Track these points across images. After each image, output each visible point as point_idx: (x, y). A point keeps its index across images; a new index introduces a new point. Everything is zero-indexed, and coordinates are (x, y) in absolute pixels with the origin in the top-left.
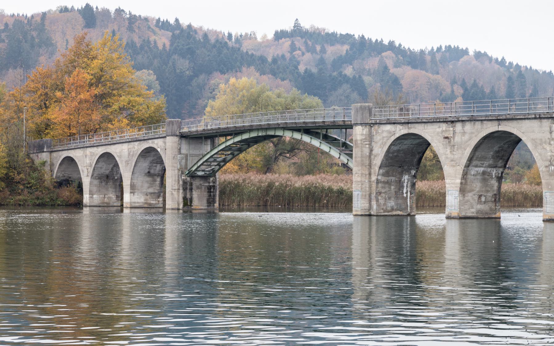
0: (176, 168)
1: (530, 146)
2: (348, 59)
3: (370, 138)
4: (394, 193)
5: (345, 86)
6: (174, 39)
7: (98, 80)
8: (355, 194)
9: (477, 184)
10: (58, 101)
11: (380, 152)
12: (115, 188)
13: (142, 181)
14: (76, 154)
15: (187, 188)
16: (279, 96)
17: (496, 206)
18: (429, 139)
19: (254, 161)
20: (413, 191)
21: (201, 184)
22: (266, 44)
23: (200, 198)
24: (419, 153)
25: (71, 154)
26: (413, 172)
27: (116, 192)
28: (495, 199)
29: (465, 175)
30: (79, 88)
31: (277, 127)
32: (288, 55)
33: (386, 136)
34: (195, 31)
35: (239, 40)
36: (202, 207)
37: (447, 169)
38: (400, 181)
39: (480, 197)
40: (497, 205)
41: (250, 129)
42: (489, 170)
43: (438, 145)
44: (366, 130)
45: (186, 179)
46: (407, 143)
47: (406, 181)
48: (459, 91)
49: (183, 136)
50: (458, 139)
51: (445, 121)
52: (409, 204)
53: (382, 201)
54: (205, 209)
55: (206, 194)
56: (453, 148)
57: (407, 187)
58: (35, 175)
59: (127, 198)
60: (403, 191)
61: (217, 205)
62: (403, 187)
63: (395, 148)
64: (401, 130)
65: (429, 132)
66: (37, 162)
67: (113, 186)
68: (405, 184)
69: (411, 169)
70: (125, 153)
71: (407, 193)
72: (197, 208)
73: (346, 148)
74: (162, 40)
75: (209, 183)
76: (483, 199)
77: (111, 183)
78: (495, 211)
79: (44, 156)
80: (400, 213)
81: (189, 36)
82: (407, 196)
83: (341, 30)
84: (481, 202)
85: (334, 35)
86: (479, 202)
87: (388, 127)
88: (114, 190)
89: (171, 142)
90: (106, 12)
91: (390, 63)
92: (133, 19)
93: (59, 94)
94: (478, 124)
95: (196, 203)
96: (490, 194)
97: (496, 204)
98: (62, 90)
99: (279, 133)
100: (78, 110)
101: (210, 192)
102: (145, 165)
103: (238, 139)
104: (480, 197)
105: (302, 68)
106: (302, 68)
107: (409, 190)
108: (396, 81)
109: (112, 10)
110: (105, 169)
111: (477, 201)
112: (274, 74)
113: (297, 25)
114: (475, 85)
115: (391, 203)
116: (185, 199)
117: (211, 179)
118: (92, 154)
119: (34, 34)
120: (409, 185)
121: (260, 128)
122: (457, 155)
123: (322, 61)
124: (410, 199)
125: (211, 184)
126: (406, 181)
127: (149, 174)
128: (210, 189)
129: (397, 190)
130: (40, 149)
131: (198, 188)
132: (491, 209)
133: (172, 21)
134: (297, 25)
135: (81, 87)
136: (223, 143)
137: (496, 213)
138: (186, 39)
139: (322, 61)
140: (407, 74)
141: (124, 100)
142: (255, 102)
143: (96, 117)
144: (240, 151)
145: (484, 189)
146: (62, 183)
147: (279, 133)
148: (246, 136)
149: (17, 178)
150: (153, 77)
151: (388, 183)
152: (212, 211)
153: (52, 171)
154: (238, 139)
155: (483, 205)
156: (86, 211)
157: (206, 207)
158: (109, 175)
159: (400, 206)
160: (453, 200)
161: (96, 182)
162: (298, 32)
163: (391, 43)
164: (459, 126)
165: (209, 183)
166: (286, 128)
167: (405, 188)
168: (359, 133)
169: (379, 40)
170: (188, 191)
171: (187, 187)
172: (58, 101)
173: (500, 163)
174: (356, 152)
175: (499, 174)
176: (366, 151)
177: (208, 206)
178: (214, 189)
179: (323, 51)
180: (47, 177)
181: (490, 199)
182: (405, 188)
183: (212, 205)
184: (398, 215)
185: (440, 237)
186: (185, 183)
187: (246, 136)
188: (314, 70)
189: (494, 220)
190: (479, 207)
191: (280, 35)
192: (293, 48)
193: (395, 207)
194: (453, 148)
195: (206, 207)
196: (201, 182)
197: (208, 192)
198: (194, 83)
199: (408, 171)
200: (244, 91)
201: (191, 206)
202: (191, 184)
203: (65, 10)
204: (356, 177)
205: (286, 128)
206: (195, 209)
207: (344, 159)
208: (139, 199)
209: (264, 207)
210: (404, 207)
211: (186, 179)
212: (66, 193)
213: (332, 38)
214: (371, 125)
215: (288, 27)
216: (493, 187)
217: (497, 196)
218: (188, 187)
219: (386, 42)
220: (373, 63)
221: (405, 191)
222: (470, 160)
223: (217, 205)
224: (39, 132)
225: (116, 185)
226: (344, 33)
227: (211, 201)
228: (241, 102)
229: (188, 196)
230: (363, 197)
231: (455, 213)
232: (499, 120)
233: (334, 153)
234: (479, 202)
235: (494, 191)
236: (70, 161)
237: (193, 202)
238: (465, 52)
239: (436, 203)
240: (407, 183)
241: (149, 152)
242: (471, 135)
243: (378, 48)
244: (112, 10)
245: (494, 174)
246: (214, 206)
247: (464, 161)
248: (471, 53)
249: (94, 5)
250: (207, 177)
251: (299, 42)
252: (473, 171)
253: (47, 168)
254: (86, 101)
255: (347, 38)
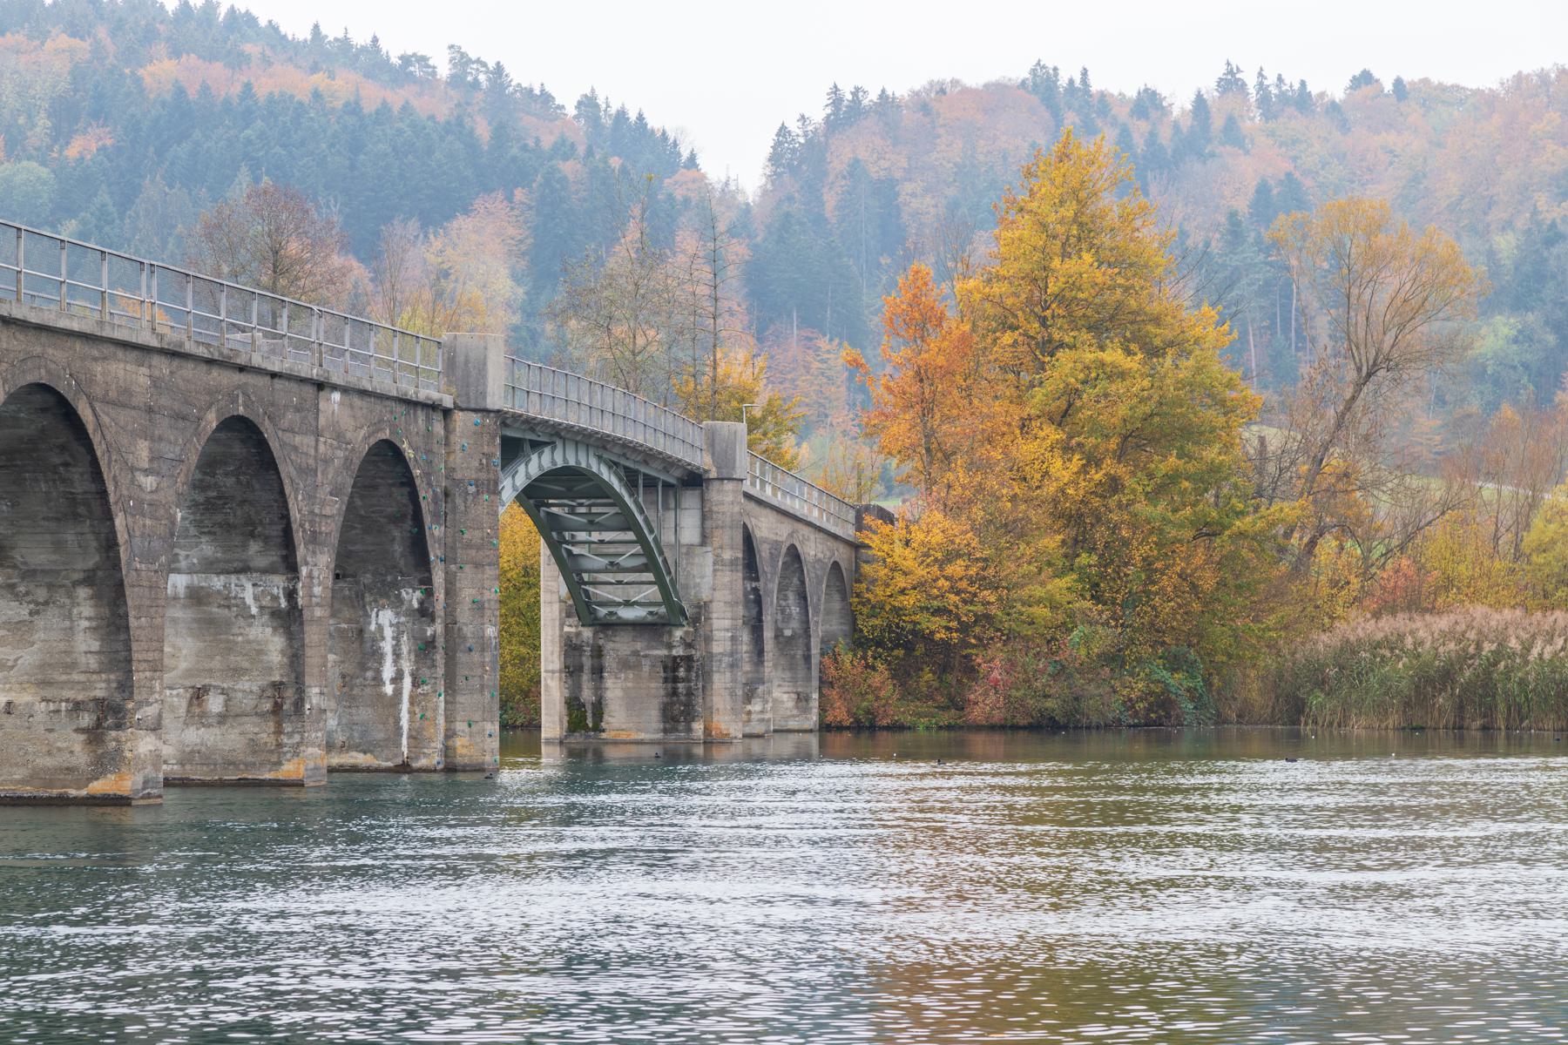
0: (556, 598)
4: (339, 682)
9: (179, 642)
12: (792, 667)
15: (580, 668)
17: (279, 732)
20: (425, 672)
21: (636, 653)
23: (631, 702)
24: (396, 520)
26: (413, 597)
27: (794, 680)
28: (277, 708)
36: (642, 736)
38: (361, 632)
39: (199, 694)
40: (287, 727)
42: (217, 582)
45: (578, 634)
47: (388, 633)
52: (405, 723)
54: (652, 743)
55: (656, 688)
57: (397, 655)
60: (378, 672)
62: (378, 656)
67: (783, 661)
68: (387, 646)
69: (396, 585)
71: (397, 679)
72: (623, 736)
75: (670, 646)
76: (215, 704)
80: (360, 759)
82: (398, 693)
84: (203, 715)
88: (787, 675)
95: (617, 720)
96: (248, 687)
97: (279, 724)
101: (675, 680)
104: (199, 694)
107: (407, 667)
111: (182, 711)
117: (678, 633)
120: (405, 649)
124: (412, 703)
125: (679, 651)
126: (388, 633)
128: (675, 669)
129: (349, 668)
131: (625, 665)
132: (254, 746)
137: (279, 763)
145: (216, 663)
152: (682, 749)
155: (217, 731)
157: (660, 736)
159: (364, 734)
165: (670, 646)
167: (389, 659)
169: (671, 136)
170: (585, 677)
175: (275, 598)
177: (665, 731)
178: (689, 669)
181: (249, 703)
182: (389, 659)
183: (681, 726)
184: (354, 769)
189: (268, 794)
190: (193, 736)
193: (340, 738)
195: (660, 736)
196: (638, 646)
197: (666, 680)
200: (980, 323)
201: (597, 728)
202: (598, 653)
206: (615, 743)
210: (381, 735)
211: (578, 634)
216: (260, 652)
217: (290, 693)
218: (587, 662)
221: (388, 672)
225: (793, 657)
226: (1448, 82)
229: (587, 695)
235: (269, 670)
237: (606, 717)
240: (397, 638)
245: (249, 600)
246: (689, 730)
250: (664, 625)
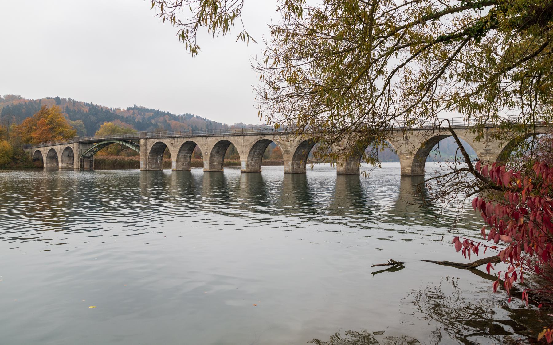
1: (199, 146)
2: (153, 117)
3: (146, 143)
5: (152, 127)
6: (90, 109)
7: (51, 122)
8: (141, 163)
10: (35, 130)
11: (149, 148)
13: (66, 159)
14: (41, 149)
16: (122, 129)
18: (166, 143)
19: (113, 152)
22: (124, 112)
25: (39, 149)
29: (178, 156)
30: (43, 125)
31: (114, 139)
32: (132, 116)
33: (152, 142)
34: (98, 107)
35: (115, 110)
37: (172, 154)
41: (104, 140)
43: (169, 146)
44: (144, 141)
46: (159, 146)
48: (190, 128)
49: (80, 143)
50: (175, 144)
51: (171, 138)
53: (150, 165)
56: (174, 147)
58: (25, 157)
59: (60, 165)
61: (93, 167)
63: (154, 147)
64: (156, 141)
65: (166, 142)
66: (26, 152)
70: (59, 149)
73: (138, 147)
74: (86, 110)
77: (54, 160)
78: (189, 168)
79: (29, 150)
81: (96, 108)
83: (151, 108)
85: (148, 109)
86: (183, 165)
87: (152, 140)
89: (75, 144)
90: (64, 100)
91: (167, 119)
92: (75, 102)
93: (35, 127)
94: (182, 139)
95: (85, 166)
98: (37, 126)
99: (115, 142)
100: (42, 133)
102: (67, 153)
103: (100, 144)
105: (136, 120)
106: (136, 120)
108: (169, 125)
109: (67, 99)
110: (52, 154)
112: (127, 122)
113: (135, 106)
114: (196, 127)
115: (154, 166)
116: (81, 165)
118: (47, 149)
119: (36, 106)
121: (108, 140)
122: (175, 149)
123: (144, 118)
127: (68, 156)
130: (27, 147)
133: (90, 103)
134: (135, 106)
135: (44, 125)
136: (95, 145)
138: (94, 110)
139: (144, 118)
140: (173, 123)
141: (61, 130)
142: (114, 131)
143: (50, 136)
144: (102, 148)
146: (35, 160)
147: (115, 142)
148: (103, 143)
149: (18, 158)
150: (82, 123)
151: (153, 159)
153: (32, 155)
154: (100, 144)
156: (45, 169)
158: (53, 156)
160: (174, 164)
161: (49, 159)
162: (135, 108)
163: (168, 112)
164: (176, 139)
166: (117, 140)
168: (142, 141)
171: (82, 161)
172: (35, 130)
173: (190, 152)
174: (141, 148)
176: (145, 148)
179: (144, 114)
180: (30, 157)
185: (170, 178)
186: (81, 159)
187: (103, 143)
188: (141, 121)
191: (129, 109)
192: (134, 113)
194: (174, 147)
198: (97, 125)
199: (160, 155)
203: (49, 98)
204: (141, 157)
205: (117, 140)
207: (137, 151)
208: (65, 165)
209: (114, 167)
212: (37, 163)
213: (147, 110)
214: (146, 139)
215: (132, 106)
219: (166, 112)
220: (161, 119)
222: (180, 151)
223: (93, 167)
224: (28, 141)
227: (91, 166)
228: (109, 131)
230: (144, 164)
231: (175, 169)
232: (189, 137)
233: (134, 149)
234: (183, 165)
236: (38, 152)
238: (193, 116)
239: (169, 165)
241: (68, 148)
242: (179, 143)
243: (163, 114)
244: (67, 99)
247: (178, 151)
248: (195, 116)
249: (60, 97)
251: (136, 111)
252: (181, 155)
253: (30, 154)
254: (46, 130)
255: (153, 110)
